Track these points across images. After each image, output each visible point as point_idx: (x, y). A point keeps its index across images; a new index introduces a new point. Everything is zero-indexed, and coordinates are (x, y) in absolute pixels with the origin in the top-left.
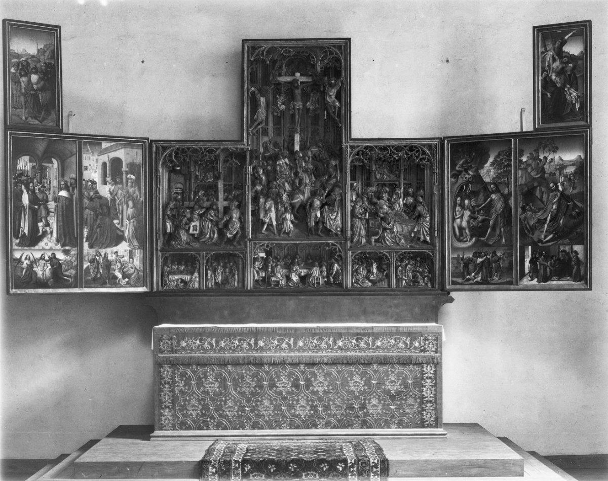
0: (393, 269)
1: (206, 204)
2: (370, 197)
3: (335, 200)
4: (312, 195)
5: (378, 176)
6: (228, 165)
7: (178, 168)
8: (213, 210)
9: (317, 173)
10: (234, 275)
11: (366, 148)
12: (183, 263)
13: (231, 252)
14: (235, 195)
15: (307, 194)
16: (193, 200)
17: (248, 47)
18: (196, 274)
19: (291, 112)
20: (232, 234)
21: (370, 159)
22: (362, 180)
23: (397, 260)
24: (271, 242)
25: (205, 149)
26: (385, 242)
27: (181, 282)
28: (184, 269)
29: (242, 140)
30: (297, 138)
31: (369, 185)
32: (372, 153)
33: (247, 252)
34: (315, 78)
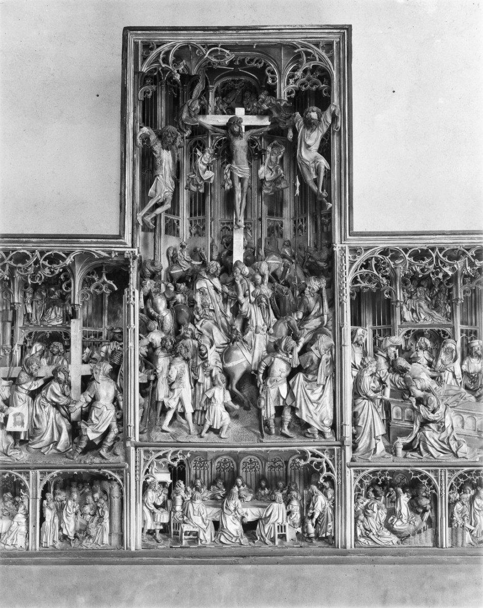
0: (443, 508)
1: (45, 370)
2: (392, 358)
3: (319, 360)
4: (268, 351)
5: (408, 316)
6: (92, 289)
8: (59, 382)
9: (279, 307)
11: (385, 252)
13: (96, 471)
14: (107, 353)
15: (260, 343)
17: (136, 44)
18: (20, 517)
19: (228, 187)
20: (97, 432)
21: (392, 279)
22: (374, 324)
23: (451, 488)
24: (181, 450)
25: (42, 253)
26: (427, 451)
29: (121, 236)
30: (239, 240)
31: (390, 332)
32: (398, 262)
33: (129, 471)
34: (275, 115)
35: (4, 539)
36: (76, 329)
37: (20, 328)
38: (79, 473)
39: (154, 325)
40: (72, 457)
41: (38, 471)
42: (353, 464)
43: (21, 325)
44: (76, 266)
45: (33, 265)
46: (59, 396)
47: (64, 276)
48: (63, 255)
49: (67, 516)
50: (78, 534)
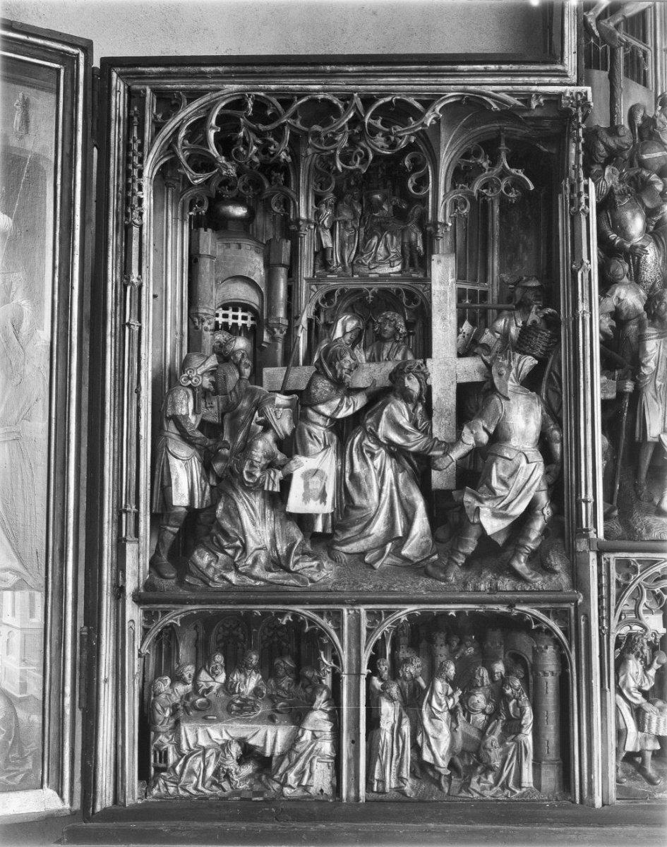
7: (240, 211)
8: (406, 396)
10: (513, 727)
12: (254, 658)
13: (503, 609)
16: (308, 361)
18: (319, 719)
25: (368, 100)
27: (241, 761)
28: (256, 691)
33: (584, 610)
35: (280, 771)
36: (443, 278)
37: (308, 280)
38: (459, 613)
39: (622, 268)
40: (442, 575)
41: (363, 609)
42: (151, 595)
43: (310, 275)
44: (443, 135)
45: (347, 129)
46: (407, 432)
47: (413, 160)
48: (417, 105)
49: (432, 716)
50: (457, 760)
